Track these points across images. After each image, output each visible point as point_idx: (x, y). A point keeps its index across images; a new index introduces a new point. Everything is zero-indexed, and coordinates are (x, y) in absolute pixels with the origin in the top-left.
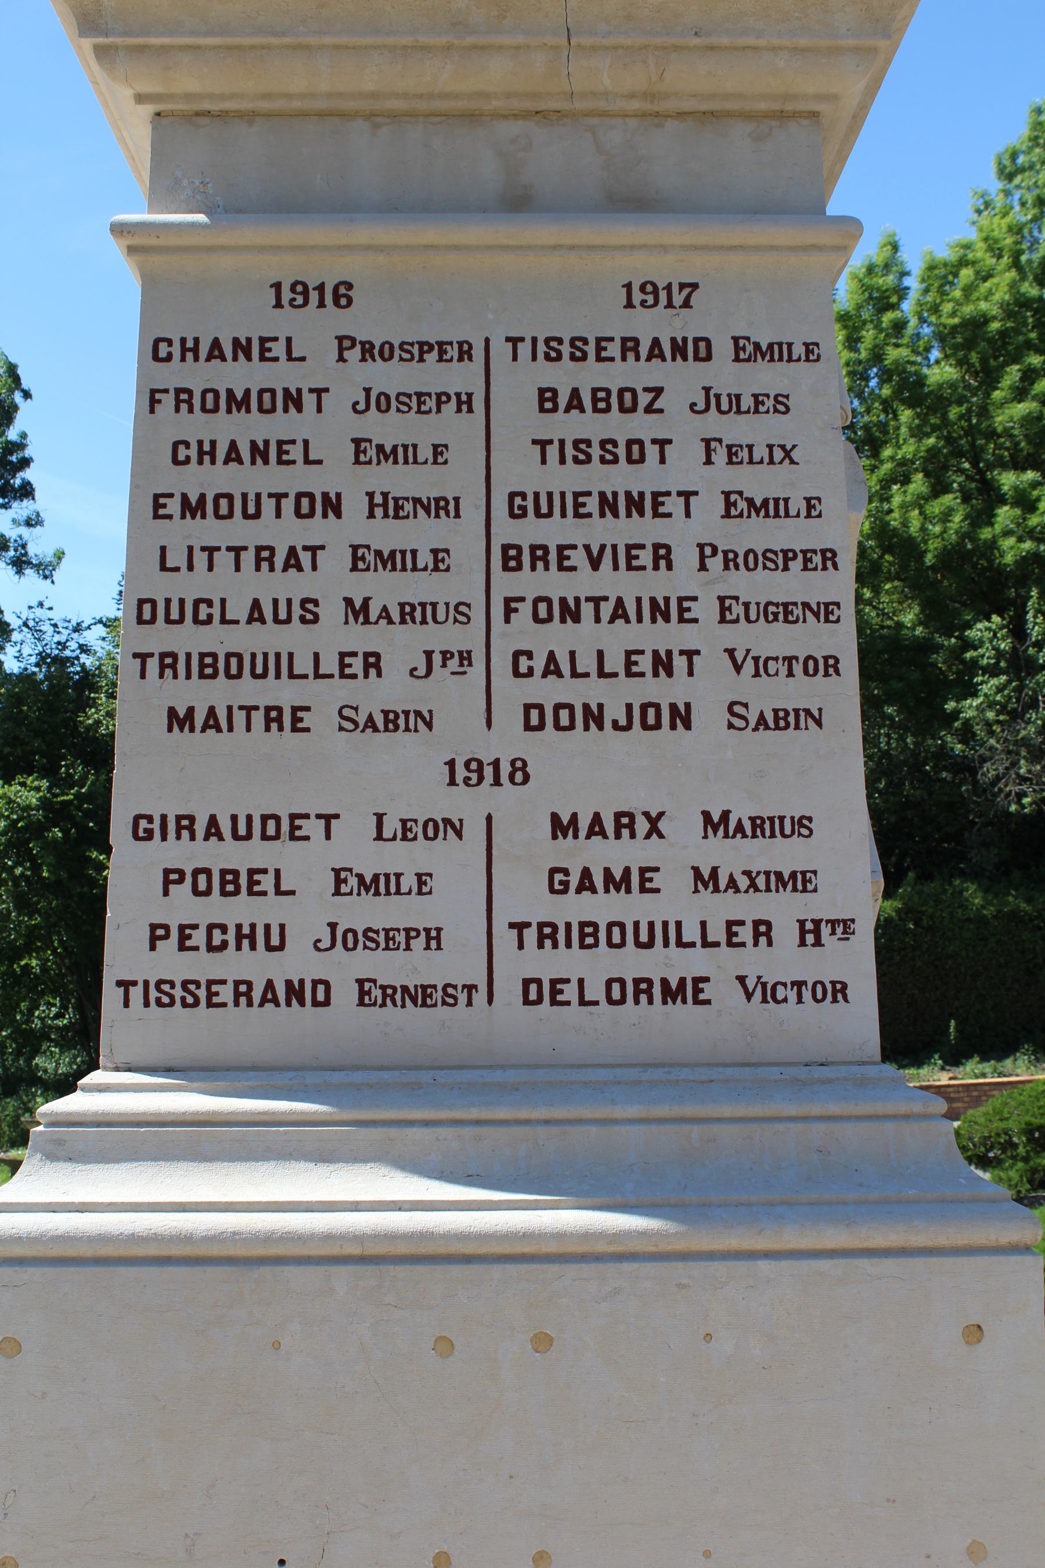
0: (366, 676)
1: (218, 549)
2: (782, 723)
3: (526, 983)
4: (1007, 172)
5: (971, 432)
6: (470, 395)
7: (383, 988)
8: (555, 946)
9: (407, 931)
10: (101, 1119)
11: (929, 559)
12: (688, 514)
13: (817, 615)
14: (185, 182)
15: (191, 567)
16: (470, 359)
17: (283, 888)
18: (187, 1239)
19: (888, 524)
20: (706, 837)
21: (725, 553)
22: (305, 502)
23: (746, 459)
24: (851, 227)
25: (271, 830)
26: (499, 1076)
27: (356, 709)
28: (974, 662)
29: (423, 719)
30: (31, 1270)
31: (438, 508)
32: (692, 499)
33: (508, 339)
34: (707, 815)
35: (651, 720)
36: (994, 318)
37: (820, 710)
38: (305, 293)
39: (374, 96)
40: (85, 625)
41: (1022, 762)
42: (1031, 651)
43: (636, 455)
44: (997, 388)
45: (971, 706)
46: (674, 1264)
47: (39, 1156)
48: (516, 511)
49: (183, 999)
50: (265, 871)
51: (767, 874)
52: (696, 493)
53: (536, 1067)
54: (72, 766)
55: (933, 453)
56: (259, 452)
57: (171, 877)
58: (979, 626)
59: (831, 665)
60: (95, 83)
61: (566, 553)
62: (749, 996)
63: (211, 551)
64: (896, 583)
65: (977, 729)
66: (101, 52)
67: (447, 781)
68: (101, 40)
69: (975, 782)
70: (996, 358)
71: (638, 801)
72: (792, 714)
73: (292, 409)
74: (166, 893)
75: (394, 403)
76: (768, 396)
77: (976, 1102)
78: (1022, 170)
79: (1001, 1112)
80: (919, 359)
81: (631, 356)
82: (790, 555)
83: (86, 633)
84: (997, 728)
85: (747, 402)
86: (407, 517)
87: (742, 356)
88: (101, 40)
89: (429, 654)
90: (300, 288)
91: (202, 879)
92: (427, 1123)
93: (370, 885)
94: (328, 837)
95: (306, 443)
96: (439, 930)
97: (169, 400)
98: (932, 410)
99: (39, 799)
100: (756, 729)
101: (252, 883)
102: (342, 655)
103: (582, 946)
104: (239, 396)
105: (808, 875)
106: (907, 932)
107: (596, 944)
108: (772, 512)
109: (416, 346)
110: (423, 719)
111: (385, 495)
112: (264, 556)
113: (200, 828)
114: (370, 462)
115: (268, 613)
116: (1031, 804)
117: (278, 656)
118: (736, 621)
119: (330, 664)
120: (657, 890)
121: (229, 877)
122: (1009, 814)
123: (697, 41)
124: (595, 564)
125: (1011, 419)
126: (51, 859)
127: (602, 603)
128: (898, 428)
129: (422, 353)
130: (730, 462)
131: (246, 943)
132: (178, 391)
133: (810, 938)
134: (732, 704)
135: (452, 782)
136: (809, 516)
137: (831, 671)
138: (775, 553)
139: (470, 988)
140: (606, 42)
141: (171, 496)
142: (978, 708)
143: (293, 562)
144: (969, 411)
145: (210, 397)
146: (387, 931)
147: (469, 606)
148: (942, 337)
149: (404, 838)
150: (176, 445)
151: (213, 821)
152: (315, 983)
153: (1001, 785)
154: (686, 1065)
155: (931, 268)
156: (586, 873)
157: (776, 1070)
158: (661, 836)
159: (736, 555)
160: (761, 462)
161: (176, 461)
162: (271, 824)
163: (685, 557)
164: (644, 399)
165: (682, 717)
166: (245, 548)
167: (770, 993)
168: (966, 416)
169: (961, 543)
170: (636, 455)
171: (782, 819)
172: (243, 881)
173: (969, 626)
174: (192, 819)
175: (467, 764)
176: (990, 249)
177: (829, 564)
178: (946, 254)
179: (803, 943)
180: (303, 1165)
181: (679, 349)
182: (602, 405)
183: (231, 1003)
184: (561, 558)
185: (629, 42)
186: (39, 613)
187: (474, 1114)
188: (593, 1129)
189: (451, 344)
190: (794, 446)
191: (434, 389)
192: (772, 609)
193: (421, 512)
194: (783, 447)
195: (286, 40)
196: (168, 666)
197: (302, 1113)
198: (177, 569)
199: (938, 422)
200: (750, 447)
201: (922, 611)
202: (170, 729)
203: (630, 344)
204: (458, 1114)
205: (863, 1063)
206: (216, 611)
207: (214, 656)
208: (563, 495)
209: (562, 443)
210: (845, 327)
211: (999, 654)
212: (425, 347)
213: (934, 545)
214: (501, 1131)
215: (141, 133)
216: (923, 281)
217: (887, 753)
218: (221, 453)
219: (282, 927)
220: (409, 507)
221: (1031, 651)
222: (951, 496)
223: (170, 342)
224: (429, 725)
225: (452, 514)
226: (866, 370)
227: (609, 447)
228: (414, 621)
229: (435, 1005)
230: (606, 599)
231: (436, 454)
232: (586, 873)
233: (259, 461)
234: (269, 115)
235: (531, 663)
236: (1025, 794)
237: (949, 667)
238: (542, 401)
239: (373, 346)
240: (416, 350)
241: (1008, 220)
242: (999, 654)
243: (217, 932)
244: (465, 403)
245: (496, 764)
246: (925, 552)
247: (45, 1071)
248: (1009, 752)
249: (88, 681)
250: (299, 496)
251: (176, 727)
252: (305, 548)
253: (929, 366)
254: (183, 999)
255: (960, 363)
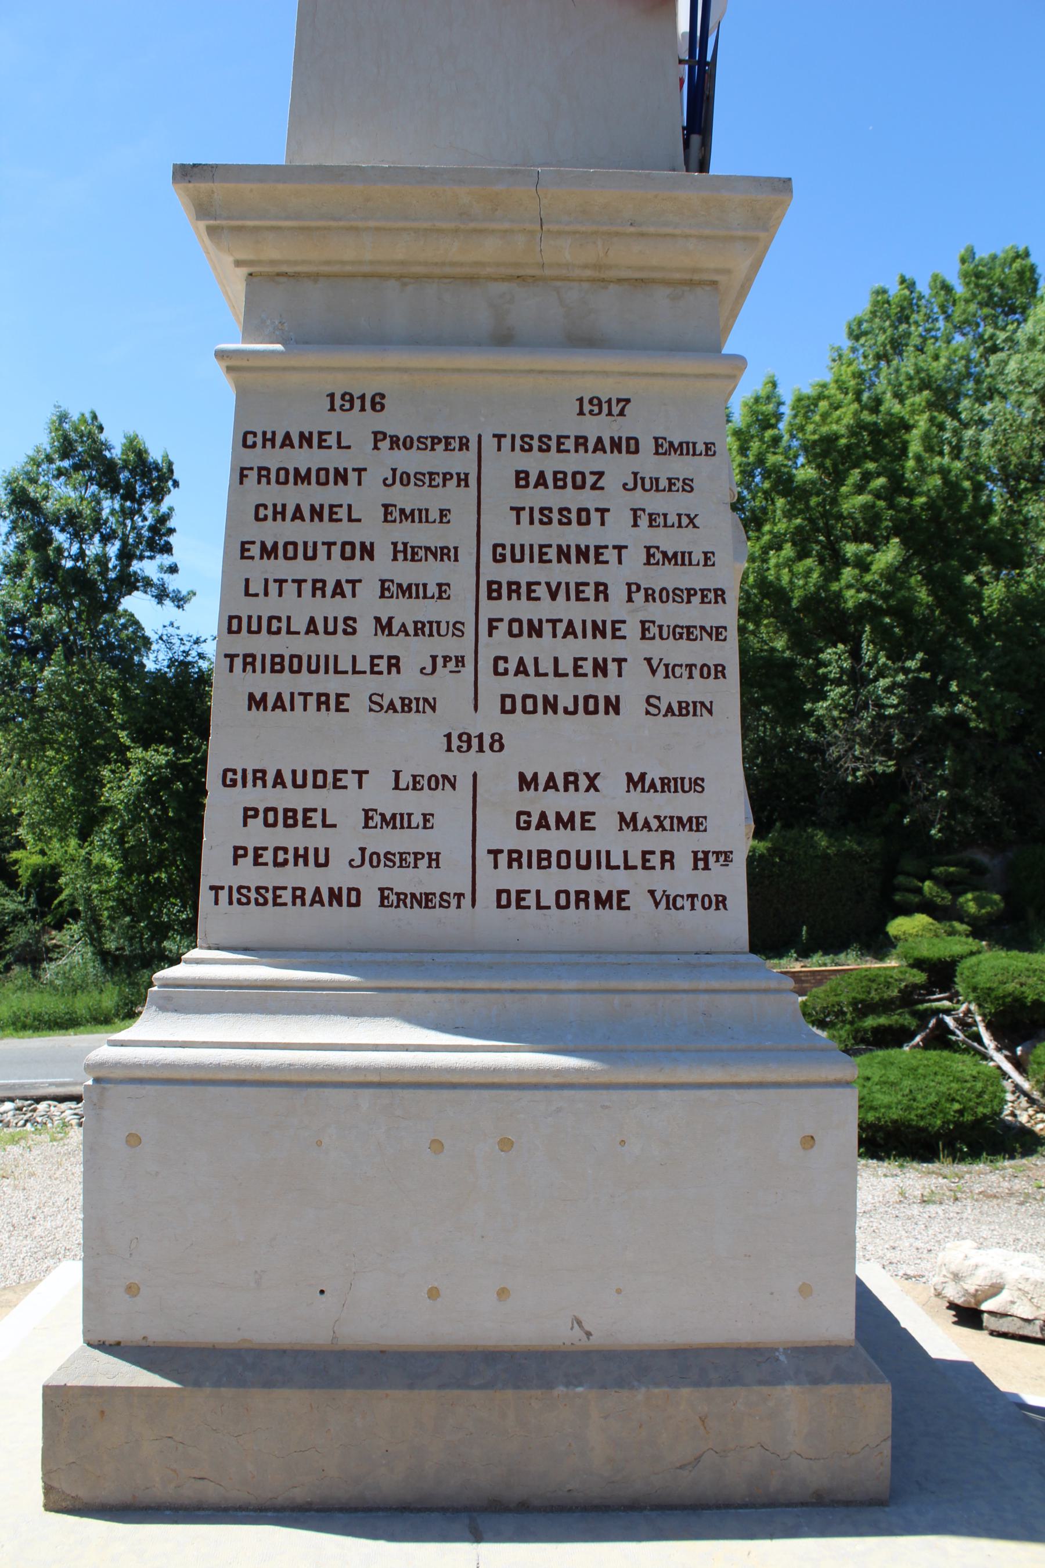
0: (389, 673)
1: (286, 581)
2: (684, 712)
3: (499, 892)
4: (856, 335)
5: (825, 515)
6: (466, 475)
7: (398, 894)
8: (520, 866)
9: (416, 854)
10: (198, 983)
11: (795, 603)
12: (620, 562)
13: (710, 635)
14: (268, 322)
15: (266, 594)
16: (467, 449)
17: (328, 822)
18: (257, 1068)
19: (766, 578)
20: (628, 791)
21: (646, 590)
22: (348, 548)
23: (662, 524)
24: (739, 362)
25: (320, 782)
26: (478, 958)
27: (382, 696)
28: (825, 676)
29: (429, 704)
30: (148, 1087)
31: (442, 554)
32: (623, 551)
33: (494, 436)
34: (629, 776)
35: (591, 708)
36: (843, 436)
37: (711, 702)
38: (352, 401)
39: (402, 263)
40: (202, 639)
41: (857, 746)
42: (865, 669)
43: (584, 519)
44: (844, 485)
45: (822, 707)
46: (600, 1092)
47: (154, 1008)
48: (498, 558)
49: (256, 900)
50: (315, 810)
51: (672, 818)
52: (626, 547)
53: (505, 952)
54: (191, 738)
55: (799, 529)
56: (316, 513)
57: (249, 814)
58: (829, 651)
59: (720, 671)
60: (208, 253)
61: (533, 587)
62: (657, 904)
63: (281, 582)
64: (772, 620)
65: (826, 723)
66: (211, 231)
67: (446, 748)
68: (212, 222)
69: (824, 760)
70: (843, 464)
71: (581, 765)
72: (691, 705)
73: (340, 483)
74: (245, 824)
75: (412, 479)
76: (678, 479)
77: (820, 983)
78: (865, 333)
79: (835, 990)
80: (790, 463)
81: (581, 449)
82: (692, 592)
83: (202, 645)
84: (840, 723)
85: (663, 483)
86: (420, 560)
87: (660, 450)
88: (212, 222)
89: (434, 658)
90: (348, 398)
91: (271, 815)
92: (427, 990)
93: (390, 821)
94: (360, 787)
95: (350, 507)
96: (438, 854)
97: (253, 475)
98: (799, 498)
99: (168, 761)
100: (665, 715)
101: (306, 818)
102: (373, 658)
103: (540, 867)
104: (303, 473)
105: (701, 820)
106: (774, 864)
107: (549, 866)
108: (679, 562)
109: (429, 440)
110: (429, 704)
111: (405, 545)
112: (318, 586)
113: (270, 778)
114: (394, 521)
115: (320, 627)
116: (862, 776)
117: (327, 657)
118: (653, 638)
119: (363, 664)
120: (593, 829)
121: (290, 814)
122: (846, 783)
123: (632, 229)
124: (554, 596)
125: (854, 507)
126: (174, 804)
127: (558, 624)
128: (774, 511)
129: (433, 444)
130: (651, 526)
131: (301, 860)
132: (260, 469)
133: (701, 864)
134: (649, 697)
135: (449, 749)
136: (706, 565)
137: (720, 675)
138: (682, 591)
139: (460, 896)
140: (567, 228)
141: (253, 543)
142: (826, 708)
143: (338, 591)
144: (824, 500)
145: (282, 473)
146: (401, 854)
147: (463, 624)
148: (805, 448)
149: (414, 788)
150: (257, 507)
151: (279, 774)
152: (350, 890)
153: (842, 762)
154: (611, 953)
155: (799, 400)
156: (543, 816)
157: (675, 956)
158: (597, 790)
159: (654, 592)
160: (673, 526)
161: (257, 519)
162: (320, 777)
163: (618, 592)
164: (590, 480)
165: (613, 706)
166: (305, 581)
167: (671, 903)
168: (822, 504)
169: (817, 593)
170: (584, 519)
171: (683, 779)
172: (300, 817)
173: (821, 650)
174: (264, 772)
175: (460, 737)
176: (840, 388)
177: (719, 599)
178: (809, 391)
179: (696, 868)
180: (339, 1018)
181: (616, 445)
182: (560, 483)
183: (290, 903)
184: (530, 591)
185: (584, 229)
186: (170, 630)
187: (461, 984)
188: (545, 997)
189: (454, 438)
190: (696, 515)
191: (441, 471)
192: (678, 630)
193: (430, 556)
194: (688, 516)
195: (341, 224)
196: (249, 663)
197: (339, 981)
198: (257, 595)
199: (802, 506)
200: (665, 515)
201: (789, 640)
202: (250, 709)
203: (581, 441)
204: (449, 984)
205: (736, 953)
206: (284, 625)
207: (282, 657)
208: (531, 546)
209: (531, 509)
210: (739, 439)
211: (842, 671)
212: (435, 440)
213: (798, 593)
214: (479, 998)
215: (239, 288)
216: (793, 409)
217: (762, 739)
218: (289, 513)
219: (327, 850)
220: (422, 553)
221: (865, 669)
222: (811, 560)
223: (255, 435)
224: (433, 708)
225: (453, 558)
226: (752, 471)
227: (565, 513)
228: (423, 634)
229: (434, 907)
230: (561, 621)
231: (442, 516)
232: (543, 816)
233: (316, 519)
234: (328, 276)
235: (506, 665)
236: (858, 769)
237: (808, 681)
238: (518, 479)
239: (398, 439)
240: (429, 442)
241: (852, 368)
242: (842, 671)
243: (280, 853)
244: (463, 480)
245: (480, 737)
246: (792, 598)
247: (171, 951)
248: (848, 740)
249: (204, 679)
250: (344, 544)
251: (254, 707)
252: (348, 581)
253: (796, 468)
254: (256, 900)
255: (819, 467)
